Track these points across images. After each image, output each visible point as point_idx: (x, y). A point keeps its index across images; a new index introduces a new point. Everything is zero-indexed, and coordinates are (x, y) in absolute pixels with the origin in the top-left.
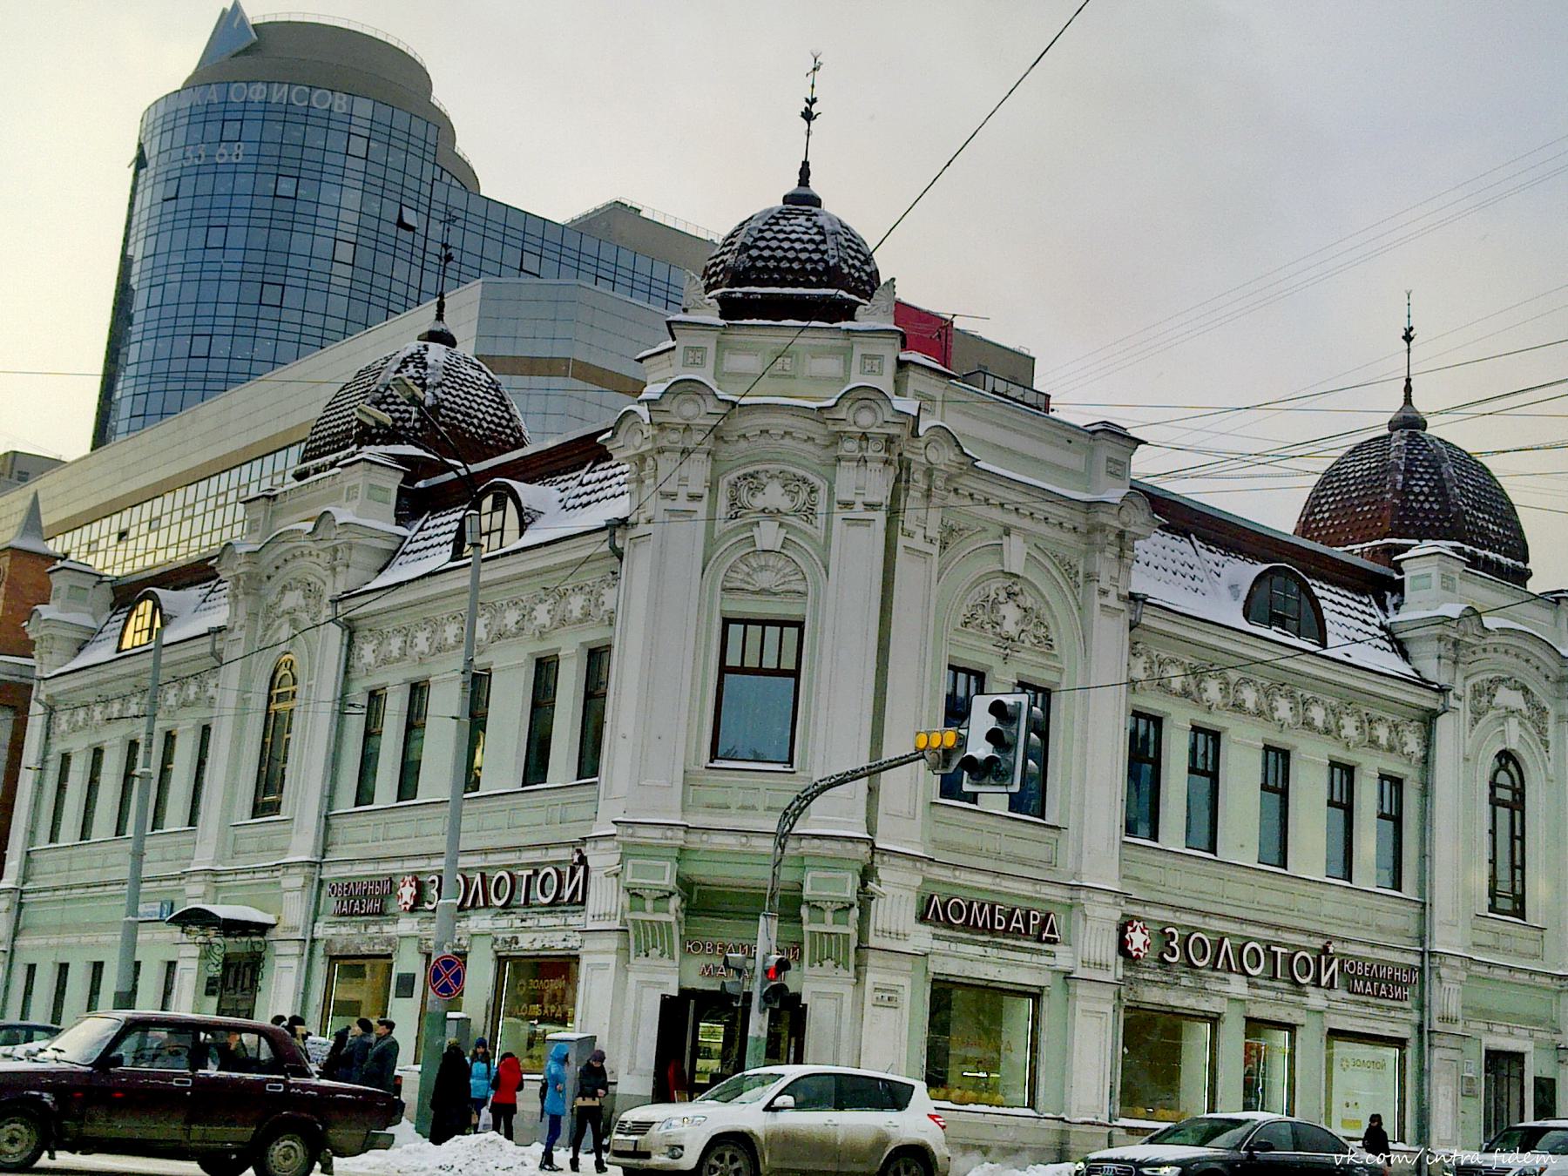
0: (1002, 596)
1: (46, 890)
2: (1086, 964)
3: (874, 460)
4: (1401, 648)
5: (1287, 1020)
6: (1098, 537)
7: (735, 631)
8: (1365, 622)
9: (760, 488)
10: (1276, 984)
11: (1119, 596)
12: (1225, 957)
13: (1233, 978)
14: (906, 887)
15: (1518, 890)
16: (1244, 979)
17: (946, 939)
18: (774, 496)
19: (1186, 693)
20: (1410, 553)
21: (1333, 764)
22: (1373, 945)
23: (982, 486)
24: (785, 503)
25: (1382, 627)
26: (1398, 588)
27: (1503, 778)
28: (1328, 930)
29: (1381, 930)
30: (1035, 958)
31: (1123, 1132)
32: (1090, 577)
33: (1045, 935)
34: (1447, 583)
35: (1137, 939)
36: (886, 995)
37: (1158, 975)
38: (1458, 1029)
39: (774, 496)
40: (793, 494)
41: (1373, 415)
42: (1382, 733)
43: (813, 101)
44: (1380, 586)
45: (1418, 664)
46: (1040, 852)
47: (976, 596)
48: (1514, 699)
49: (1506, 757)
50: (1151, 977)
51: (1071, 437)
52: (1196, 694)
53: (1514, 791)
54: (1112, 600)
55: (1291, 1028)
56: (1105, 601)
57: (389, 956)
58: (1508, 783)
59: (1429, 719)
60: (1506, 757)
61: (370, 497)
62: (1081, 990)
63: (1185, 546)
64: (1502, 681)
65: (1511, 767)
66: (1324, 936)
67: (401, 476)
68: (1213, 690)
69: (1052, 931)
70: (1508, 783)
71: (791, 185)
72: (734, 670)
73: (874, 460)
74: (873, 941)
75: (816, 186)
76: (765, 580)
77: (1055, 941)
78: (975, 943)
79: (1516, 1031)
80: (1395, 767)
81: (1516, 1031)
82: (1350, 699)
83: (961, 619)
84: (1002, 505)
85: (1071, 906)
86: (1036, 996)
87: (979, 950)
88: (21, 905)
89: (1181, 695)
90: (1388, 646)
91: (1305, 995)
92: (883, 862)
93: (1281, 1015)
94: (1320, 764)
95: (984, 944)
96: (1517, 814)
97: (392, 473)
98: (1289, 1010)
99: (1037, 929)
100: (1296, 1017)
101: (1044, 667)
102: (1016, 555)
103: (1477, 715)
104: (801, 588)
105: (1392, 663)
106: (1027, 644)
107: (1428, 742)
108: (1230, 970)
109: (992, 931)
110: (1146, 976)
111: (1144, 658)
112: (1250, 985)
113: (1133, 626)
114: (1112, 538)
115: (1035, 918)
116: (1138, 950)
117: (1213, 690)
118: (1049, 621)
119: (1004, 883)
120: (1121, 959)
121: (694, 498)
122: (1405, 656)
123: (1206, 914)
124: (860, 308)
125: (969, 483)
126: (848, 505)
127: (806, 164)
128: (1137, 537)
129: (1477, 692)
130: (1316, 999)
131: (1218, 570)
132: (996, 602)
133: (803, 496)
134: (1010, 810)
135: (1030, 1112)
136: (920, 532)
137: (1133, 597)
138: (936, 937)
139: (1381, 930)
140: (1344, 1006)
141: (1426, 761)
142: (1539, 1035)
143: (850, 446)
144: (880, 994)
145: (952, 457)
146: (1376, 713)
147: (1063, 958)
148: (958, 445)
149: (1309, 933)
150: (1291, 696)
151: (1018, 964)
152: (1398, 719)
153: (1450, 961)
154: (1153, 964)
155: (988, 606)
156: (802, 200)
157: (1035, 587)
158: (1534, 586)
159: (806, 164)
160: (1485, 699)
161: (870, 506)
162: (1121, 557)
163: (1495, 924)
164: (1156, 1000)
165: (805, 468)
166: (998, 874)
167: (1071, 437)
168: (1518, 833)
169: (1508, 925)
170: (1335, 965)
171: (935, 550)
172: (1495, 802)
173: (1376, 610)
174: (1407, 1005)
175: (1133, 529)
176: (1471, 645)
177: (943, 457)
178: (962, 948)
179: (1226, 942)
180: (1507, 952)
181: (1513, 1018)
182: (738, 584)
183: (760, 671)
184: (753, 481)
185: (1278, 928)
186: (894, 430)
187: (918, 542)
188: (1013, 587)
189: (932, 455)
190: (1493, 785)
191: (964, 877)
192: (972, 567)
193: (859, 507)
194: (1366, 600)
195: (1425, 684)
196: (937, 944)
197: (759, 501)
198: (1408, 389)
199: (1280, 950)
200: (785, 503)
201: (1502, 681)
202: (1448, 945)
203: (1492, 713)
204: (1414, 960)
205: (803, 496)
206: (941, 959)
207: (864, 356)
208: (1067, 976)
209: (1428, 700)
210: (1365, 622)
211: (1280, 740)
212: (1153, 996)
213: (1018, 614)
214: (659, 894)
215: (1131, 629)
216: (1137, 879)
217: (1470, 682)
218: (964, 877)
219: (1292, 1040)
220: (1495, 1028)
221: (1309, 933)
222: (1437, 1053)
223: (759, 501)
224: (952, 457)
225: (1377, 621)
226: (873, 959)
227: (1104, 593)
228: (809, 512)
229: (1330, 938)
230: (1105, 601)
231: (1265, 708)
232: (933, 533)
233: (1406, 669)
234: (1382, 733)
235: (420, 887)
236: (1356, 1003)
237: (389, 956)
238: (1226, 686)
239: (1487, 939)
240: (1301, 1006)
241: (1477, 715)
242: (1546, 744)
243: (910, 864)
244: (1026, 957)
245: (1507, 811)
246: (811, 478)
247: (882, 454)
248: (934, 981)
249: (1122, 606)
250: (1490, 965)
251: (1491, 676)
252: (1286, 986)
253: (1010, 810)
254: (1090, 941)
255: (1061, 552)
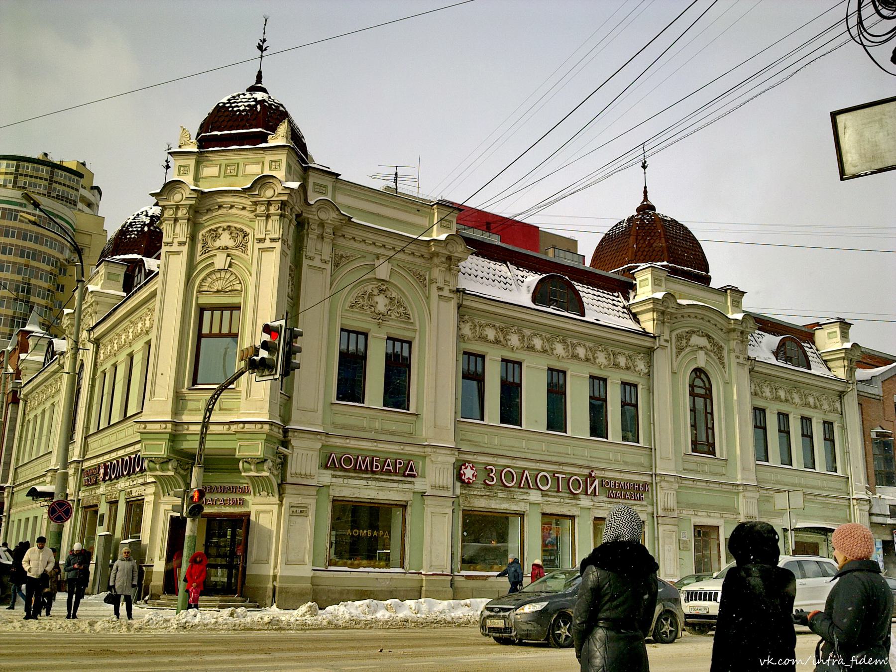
0: (376, 292)
1: (24, 483)
2: (434, 487)
3: (275, 215)
4: (635, 317)
5: (568, 513)
6: (436, 260)
7: (207, 314)
8: (614, 305)
9: (218, 236)
10: (560, 494)
11: (450, 291)
12: (526, 482)
13: (531, 491)
14: (312, 449)
15: (711, 441)
16: (539, 492)
17: (340, 477)
18: (225, 240)
19: (497, 342)
20: (639, 269)
21: (592, 378)
22: (621, 472)
23: (361, 233)
24: (231, 243)
25: (624, 307)
26: (633, 287)
27: (698, 382)
28: (592, 464)
29: (626, 463)
30: (401, 485)
31: (463, 579)
32: (433, 281)
33: (407, 472)
34: (656, 282)
35: (468, 473)
36: (299, 510)
37: (484, 492)
38: (675, 514)
39: (225, 240)
40: (234, 239)
41: (628, 209)
42: (622, 361)
43: (264, 40)
44: (626, 287)
45: (643, 325)
46: (405, 428)
47: (358, 291)
48: (703, 342)
49: (699, 372)
50: (479, 493)
51: (420, 208)
52: (504, 342)
53: (706, 389)
54: (446, 292)
55: (572, 517)
56: (441, 293)
57: (96, 506)
58: (702, 385)
59: (649, 352)
60: (699, 372)
61: (108, 279)
62: (428, 501)
63: (504, 268)
64: (694, 332)
65: (703, 376)
66: (588, 467)
67: (126, 268)
68: (514, 340)
69: (411, 470)
70: (702, 385)
71: (638, 201)
72: (207, 336)
73: (275, 215)
74: (289, 479)
75: (652, 200)
76: (218, 286)
77: (414, 476)
78: (361, 478)
79: (712, 515)
80: (630, 378)
81: (712, 515)
82: (600, 343)
83: (348, 304)
84: (374, 243)
85: (425, 457)
86: (404, 507)
87: (364, 482)
88: (13, 494)
89: (494, 343)
90: (627, 316)
91: (579, 499)
92: (295, 436)
93: (565, 511)
94: (542, 369)
95: (367, 479)
96: (708, 401)
97: (120, 267)
98: (570, 508)
99: (406, 470)
100: (574, 511)
101: (404, 329)
102: (383, 271)
103: (680, 350)
104: (239, 288)
105: (631, 324)
106: (393, 317)
107: (650, 365)
108: (529, 487)
109: (373, 472)
110: (475, 493)
111: (469, 324)
112: (543, 495)
113: (460, 306)
114: (444, 260)
115: (400, 463)
116: (469, 478)
117: (514, 340)
118: (407, 304)
119: (380, 445)
120: (458, 484)
121: (181, 244)
122: (638, 322)
123: (514, 458)
124: (270, 137)
125: (350, 231)
126: (260, 241)
127: (260, 72)
128: (460, 260)
129: (679, 338)
130: (585, 502)
131: (522, 279)
132: (371, 295)
133: (240, 239)
134: (384, 405)
135: (401, 570)
136: (318, 258)
137: (458, 291)
138: (334, 476)
139: (626, 463)
140: (603, 505)
141: (649, 375)
142: (725, 516)
143: (261, 209)
144: (295, 509)
145: (335, 216)
146: (617, 350)
147: (419, 485)
148: (338, 210)
149: (581, 467)
150: (564, 342)
151: (390, 489)
152: (631, 353)
153: (667, 479)
154: (480, 486)
155: (366, 297)
156: (646, 208)
157: (395, 285)
158: (714, 284)
159: (260, 72)
160: (684, 342)
161: (273, 240)
162: (449, 269)
163: (695, 459)
164: (483, 505)
165: (243, 224)
166: (376, 441)
167: (420, 208)
168: (709, 411)
169: (702, 458)
170: (596, 482)
171: (328, 266)
172: (692, 394)
173: (621, 299)
174: (644, 503)
175: (456, 254)
176: (672, 314)
177: (330, 216)
178: (351, 481)
179: (526, 472)
180: (704, 472)
181: (710, 508)
182: (206, 289)
183: (220, 335)
184: (215, 234)
185: (560, 464)
186: (285, 198)
187: (317, 262)
188: (383, 286)
189: (323, 216)
190: (692, 386)
191: (353, 443)
192: (349, 275)
193: (268, 241)
194: (616, 294)
195: (645, 333)
196: (334, 480)
197: (218, 244)
198: (645, 192)
199: (561, 476)
200: (231, 243)
201: (694, 332)
202: (664, 470)
203: (688, 349)
204: (647, 479)
205: (240, 239)
206: (338, 489)
207: (271, 161)
208: (423, 494)
209: (647, 343)
210: (614, 305)
211: (557, 365)
212: (481, 503)
213: (387, 301)
214: (162, 460)
215: (458, 308)
216: (469, 441)
217: (674, 334)
218: (353, 443)
219: (522, 520)
220: (699, 513)
221: (581, 467)
222: (661, 528)
223: (218, 244)
224: (335, 216)
225: (622, 305)
226: (289, 489)
227: (440, 289)
228: (243, 247)
229: (592, 469)
230: (441, 293)
231: (547, 348)
232: (326, 257)
233: (635, 326)
234: (622, 361)
235: (106, 467)
236: (610, 503)
237: (96, 506)
238: (522, 338)
239: (692, 466)
240: (576, 505)
241: (680, 350)
242: (723, 364)
243: (312, 436)
244: (395, 485)
245: (702, 399)
246: (246, 229)
247: (279, 211)
248: (334, 501)
249: (452, 295)
250: (694, 480)
251: (687, 330)
252: (567, 495)
253: (502, 422)
254: (437, 473)
255: (414, 268)
